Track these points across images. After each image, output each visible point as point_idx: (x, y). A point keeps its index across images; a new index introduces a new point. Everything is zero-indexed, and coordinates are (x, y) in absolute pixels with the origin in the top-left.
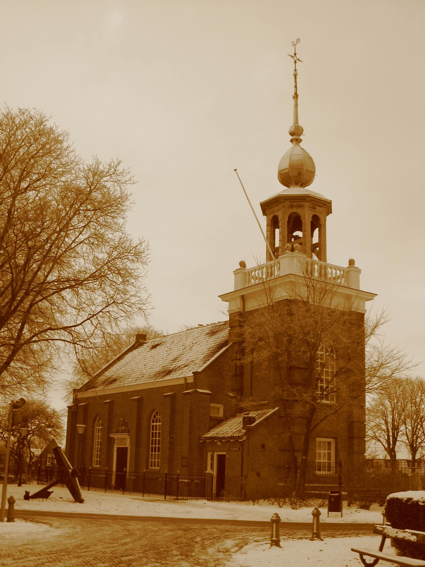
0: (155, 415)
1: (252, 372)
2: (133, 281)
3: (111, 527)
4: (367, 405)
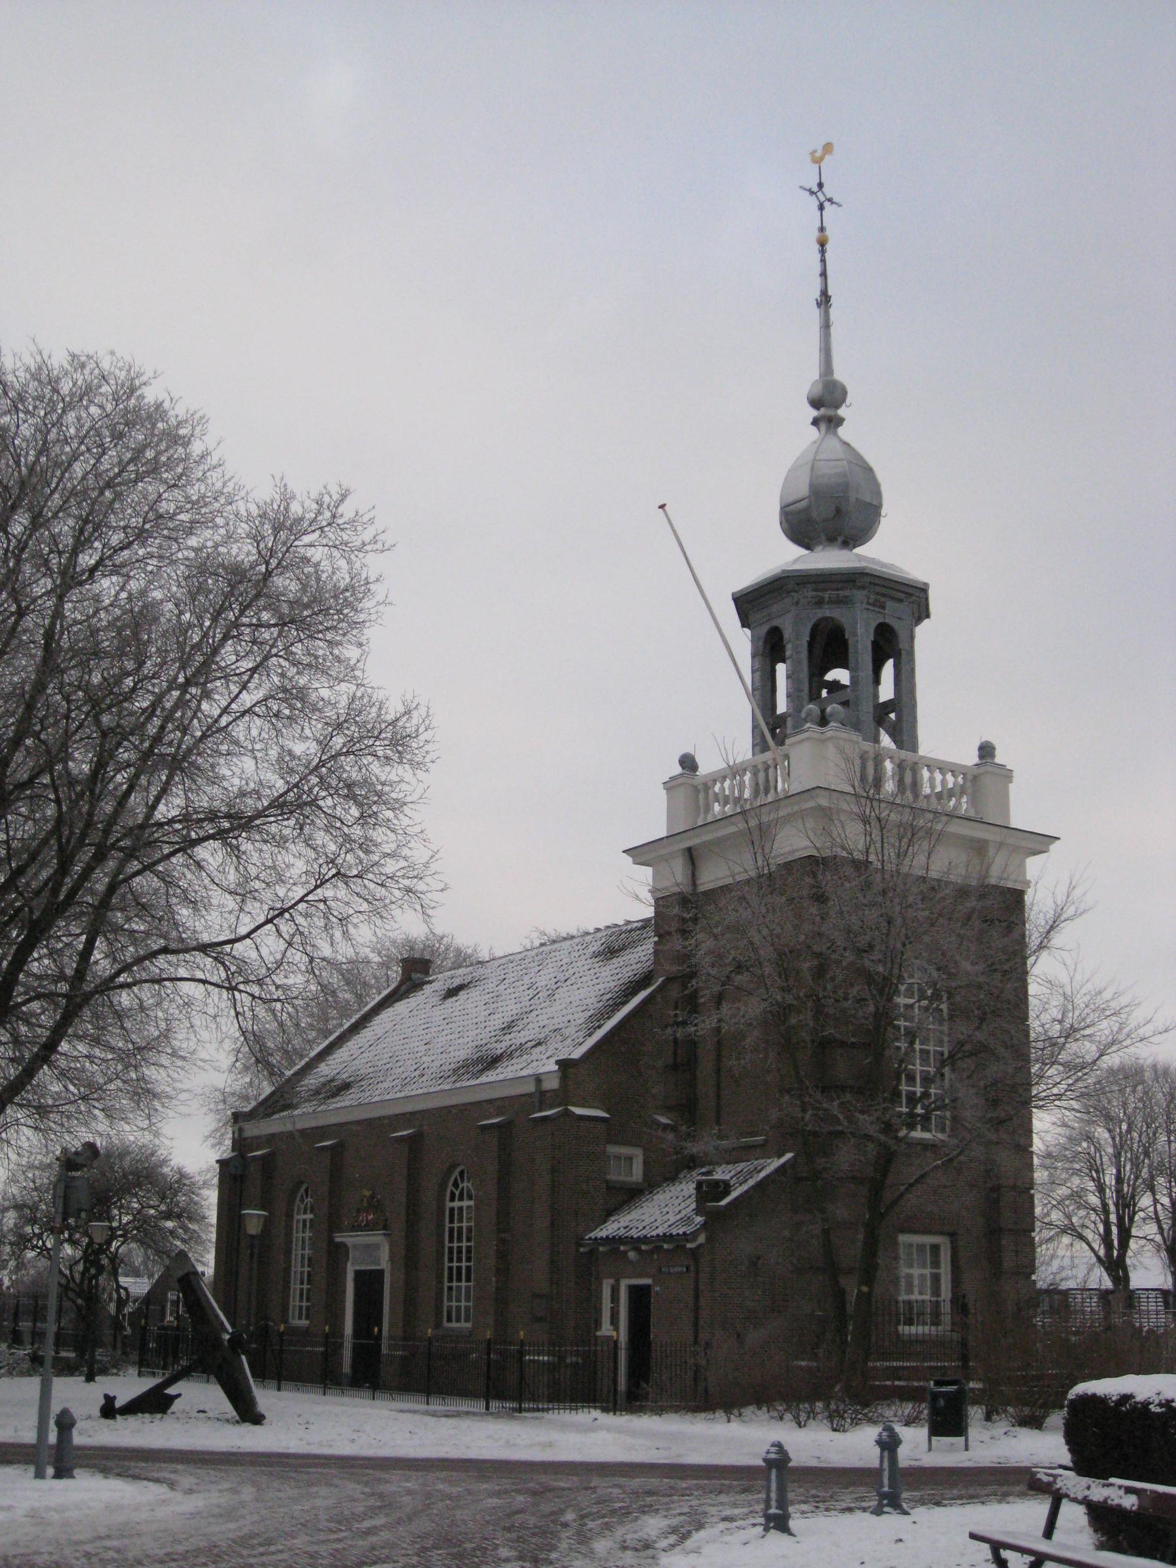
0: (456, 1180)
1: (719, 1058)
2: (389, 814)
3: (336, 1486)
4: (1038, 1145)
